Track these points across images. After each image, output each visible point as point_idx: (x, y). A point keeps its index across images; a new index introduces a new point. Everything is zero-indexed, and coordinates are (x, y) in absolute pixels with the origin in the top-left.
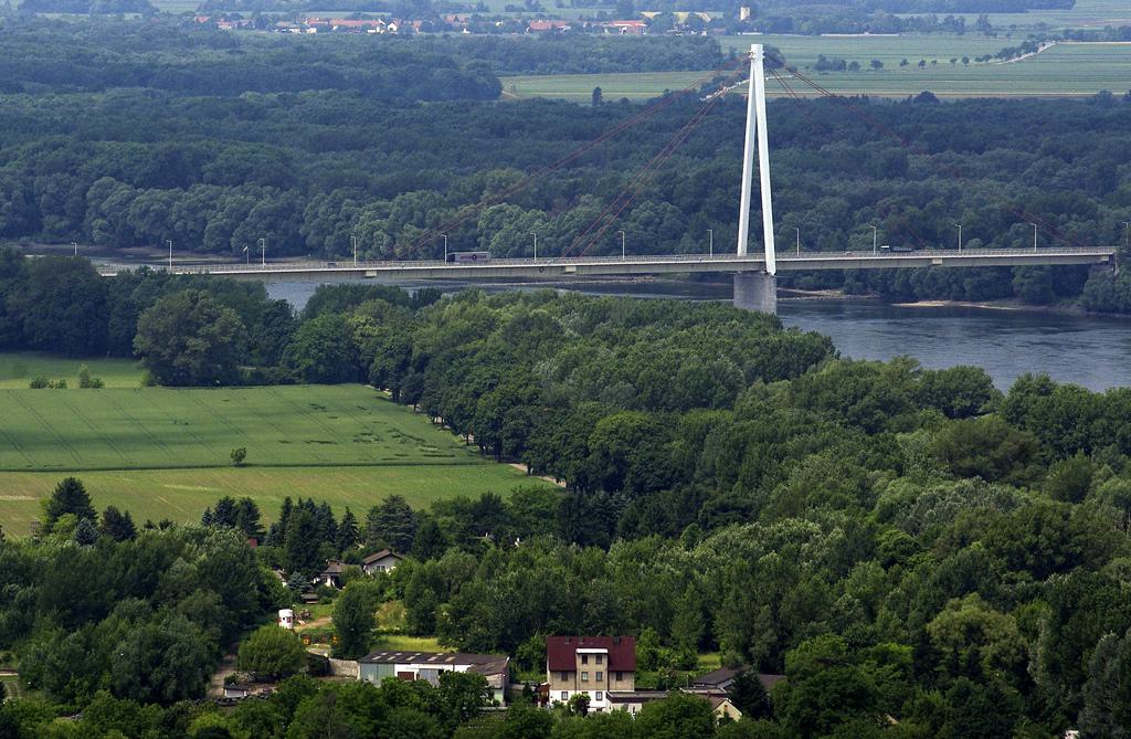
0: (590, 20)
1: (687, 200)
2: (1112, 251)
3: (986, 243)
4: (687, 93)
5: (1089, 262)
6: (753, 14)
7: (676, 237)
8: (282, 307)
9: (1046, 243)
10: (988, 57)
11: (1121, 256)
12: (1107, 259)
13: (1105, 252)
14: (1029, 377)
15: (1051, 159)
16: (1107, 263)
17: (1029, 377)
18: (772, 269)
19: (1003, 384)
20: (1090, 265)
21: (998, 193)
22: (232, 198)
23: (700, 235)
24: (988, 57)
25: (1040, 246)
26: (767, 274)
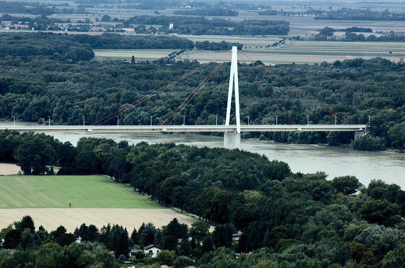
0: (113, 27)
1: (198, 103)
2: (364, 126)
3: (315, 123)
4: (98, 36)
5: (355, 130)
6: (175, 27)
7: (195, 118)
8: (68, 145)
9: (339, 123)
10: (269, 46)
11: (367, 128)
12: (362, 129)
13: (361, 127)
14: (374, 180)
15: (328, 90)
16: (362, 131)
17: (374, 180)
18: (239, 131)
19: (365, 183)
20: (355, 132)
21: (317, 106)
22: (22, 98)
23: (205, 117)
24: (269, 46)
25: (337, 124)
26: (237, 133)
